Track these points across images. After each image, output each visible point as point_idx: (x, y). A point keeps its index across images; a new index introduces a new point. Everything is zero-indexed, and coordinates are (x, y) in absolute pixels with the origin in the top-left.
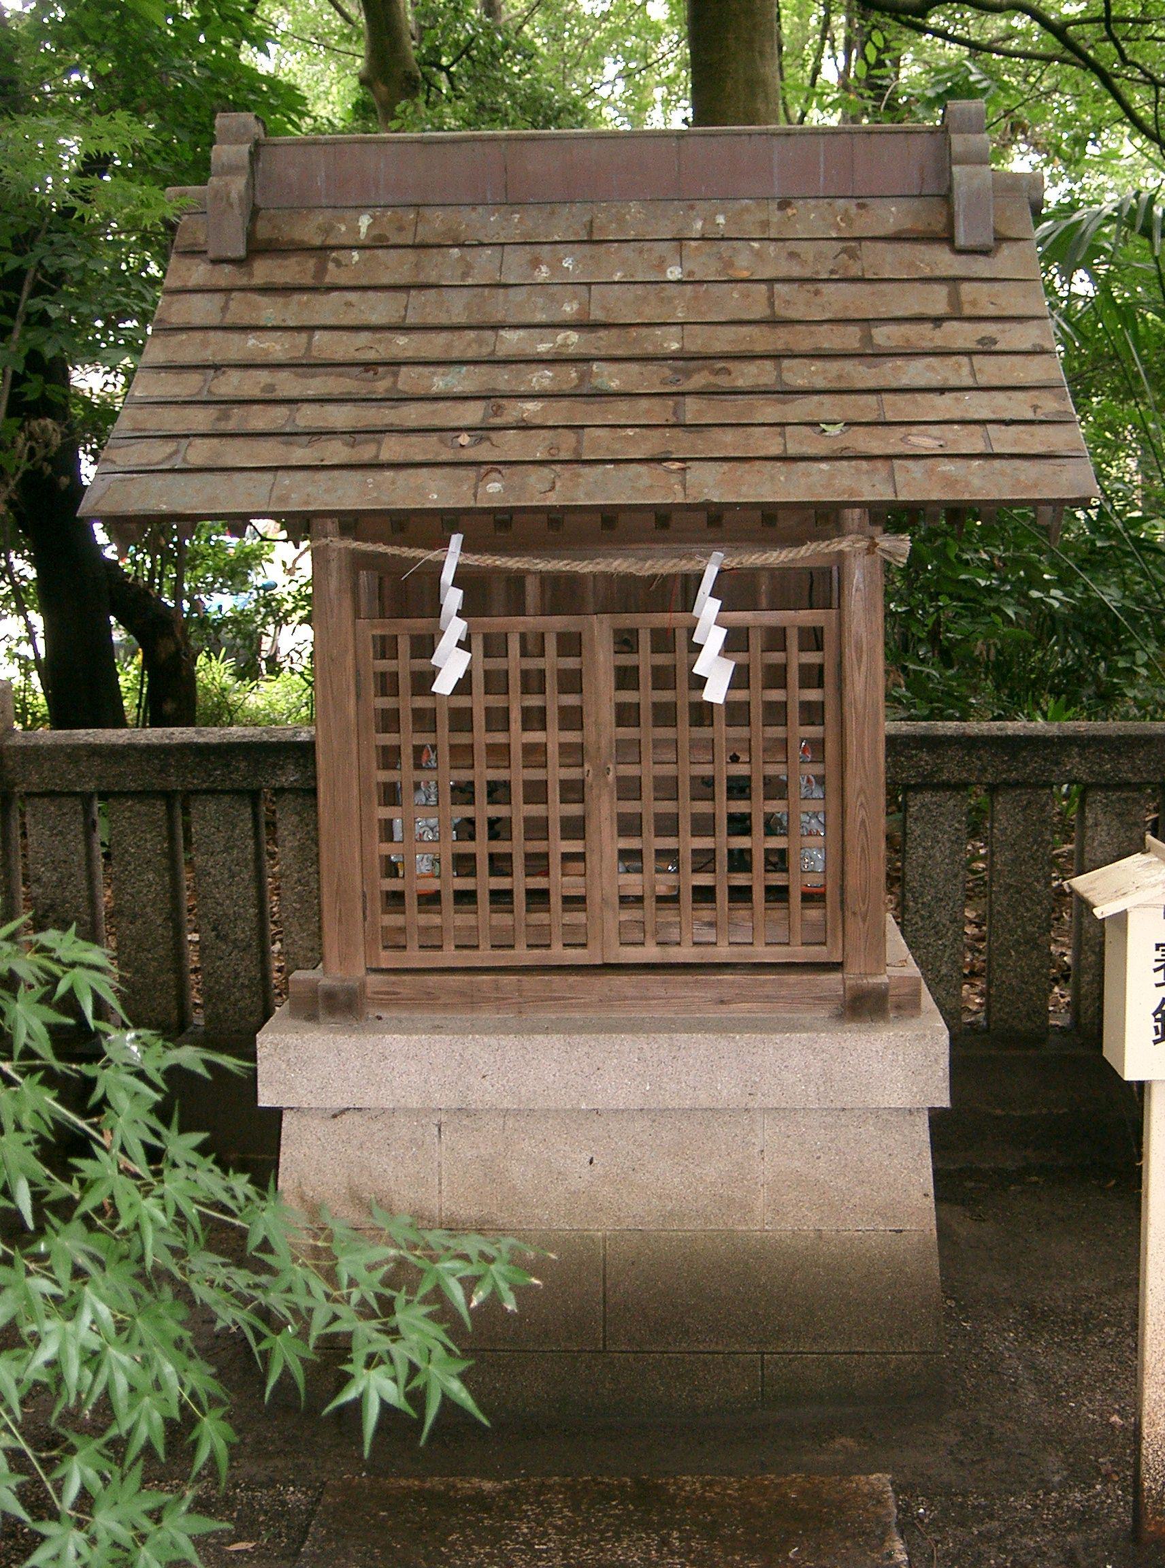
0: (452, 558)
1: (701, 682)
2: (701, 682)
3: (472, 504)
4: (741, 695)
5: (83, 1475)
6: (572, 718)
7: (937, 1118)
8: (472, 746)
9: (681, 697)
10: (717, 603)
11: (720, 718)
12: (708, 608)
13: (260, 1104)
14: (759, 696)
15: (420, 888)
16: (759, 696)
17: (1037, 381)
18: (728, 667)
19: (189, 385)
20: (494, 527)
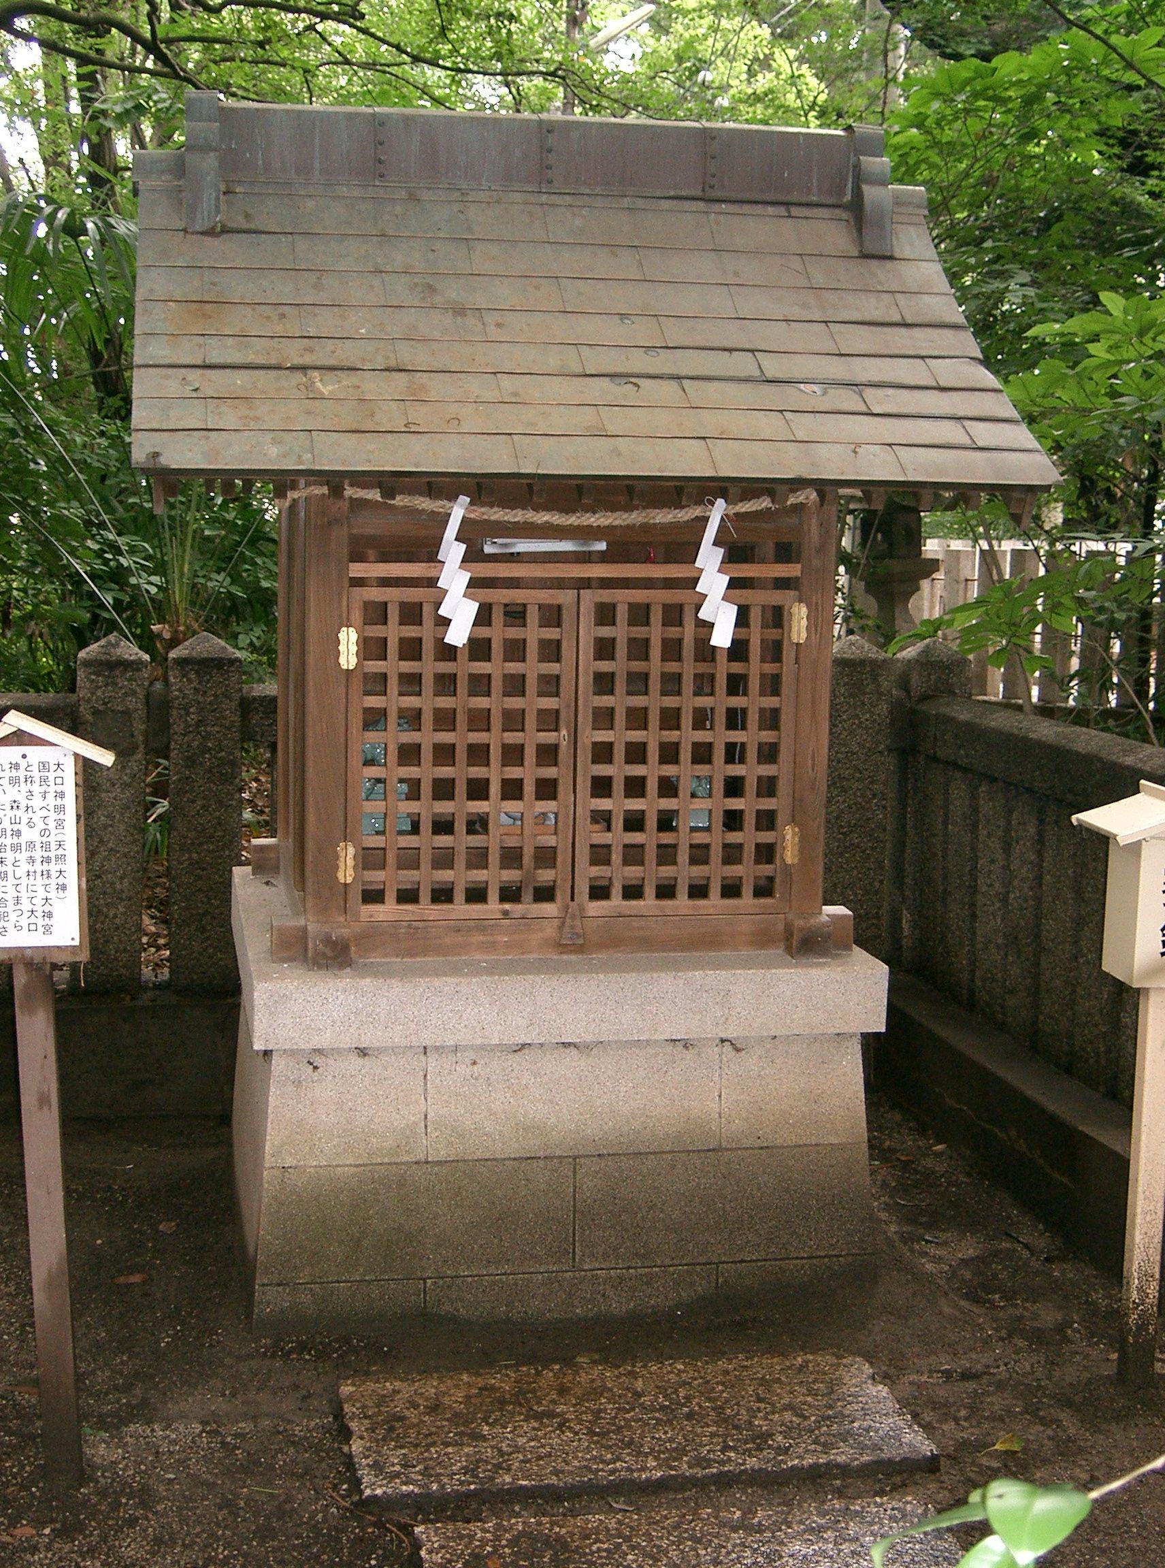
0: (458, 512)
1: (446, 622)
2: (446, 622)
3: (516, 471)
4: (484, 632)
5: (280, 1495)
6: (551, 651)
7: (870, 1042)
8: (680, 675)
9: (426, 632)
10: (720, 552)
11: (463, 657)
12: (709, 557)
13: (883, 1030)
14: (498, 633)
15: (470, 810)
16: (498, 633)
17: (803, 376)
18: (472, 608)
19: (772, 366)
20: (482, 487)
